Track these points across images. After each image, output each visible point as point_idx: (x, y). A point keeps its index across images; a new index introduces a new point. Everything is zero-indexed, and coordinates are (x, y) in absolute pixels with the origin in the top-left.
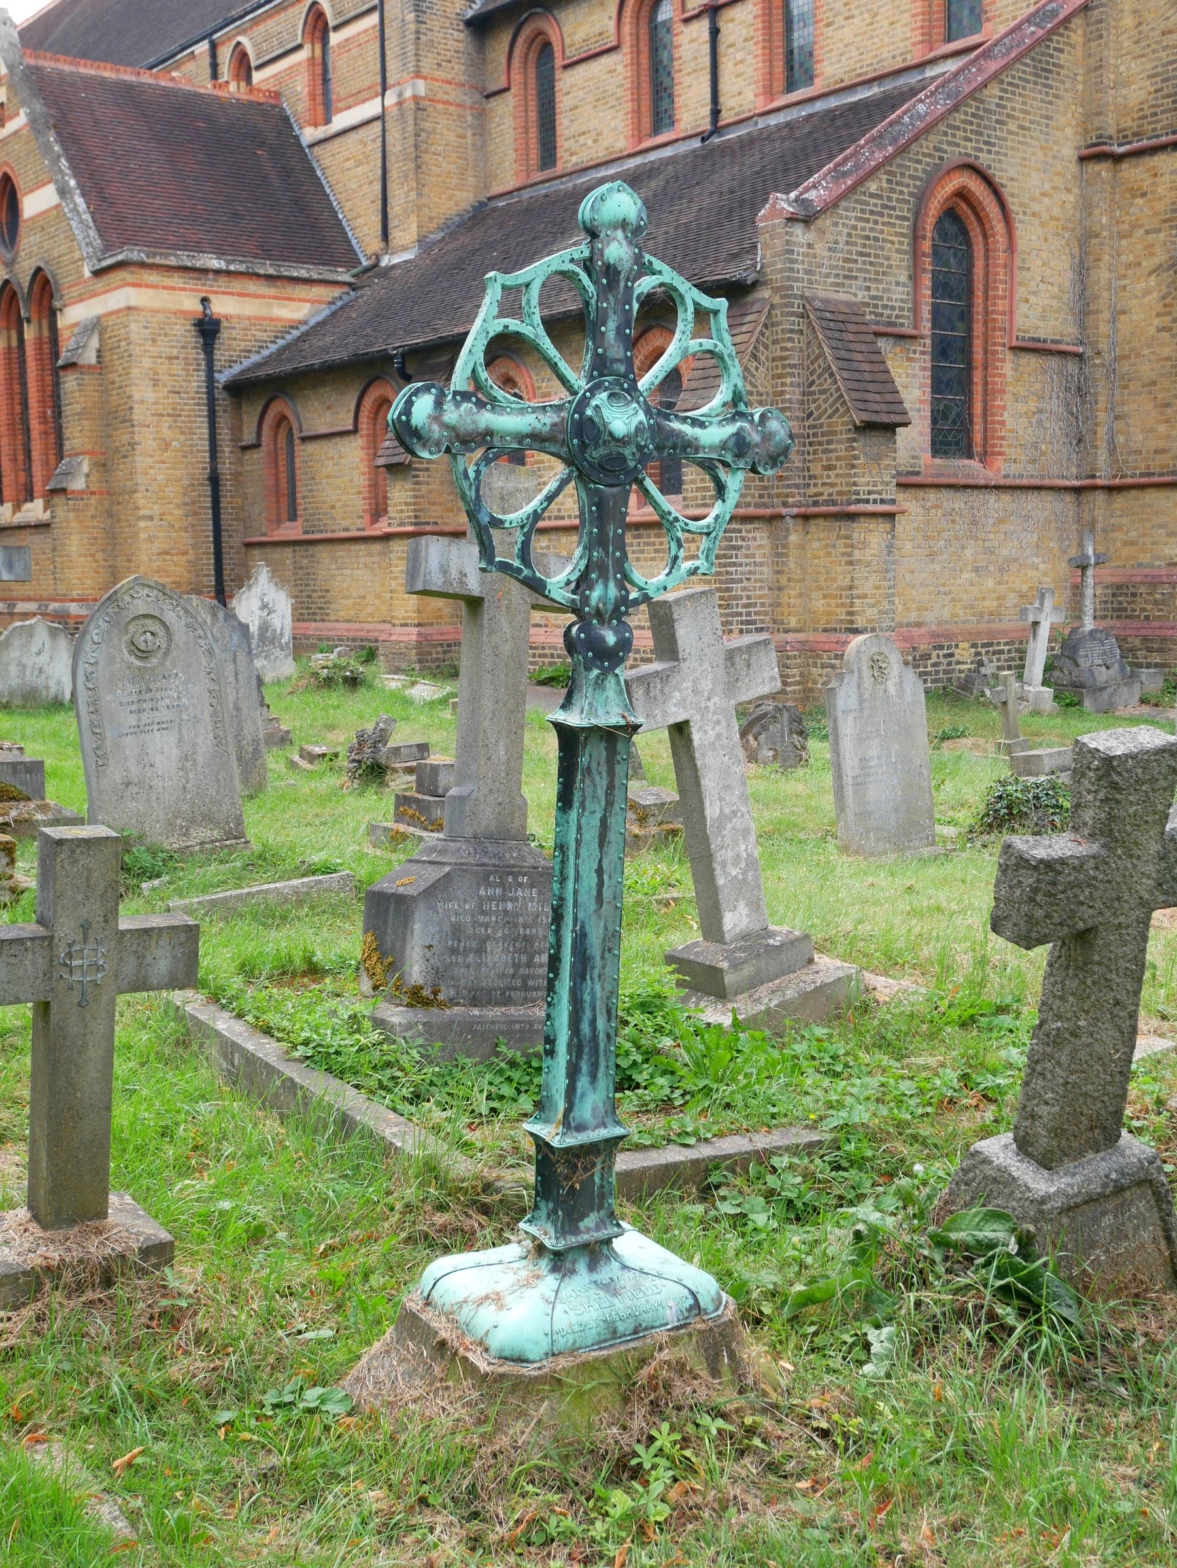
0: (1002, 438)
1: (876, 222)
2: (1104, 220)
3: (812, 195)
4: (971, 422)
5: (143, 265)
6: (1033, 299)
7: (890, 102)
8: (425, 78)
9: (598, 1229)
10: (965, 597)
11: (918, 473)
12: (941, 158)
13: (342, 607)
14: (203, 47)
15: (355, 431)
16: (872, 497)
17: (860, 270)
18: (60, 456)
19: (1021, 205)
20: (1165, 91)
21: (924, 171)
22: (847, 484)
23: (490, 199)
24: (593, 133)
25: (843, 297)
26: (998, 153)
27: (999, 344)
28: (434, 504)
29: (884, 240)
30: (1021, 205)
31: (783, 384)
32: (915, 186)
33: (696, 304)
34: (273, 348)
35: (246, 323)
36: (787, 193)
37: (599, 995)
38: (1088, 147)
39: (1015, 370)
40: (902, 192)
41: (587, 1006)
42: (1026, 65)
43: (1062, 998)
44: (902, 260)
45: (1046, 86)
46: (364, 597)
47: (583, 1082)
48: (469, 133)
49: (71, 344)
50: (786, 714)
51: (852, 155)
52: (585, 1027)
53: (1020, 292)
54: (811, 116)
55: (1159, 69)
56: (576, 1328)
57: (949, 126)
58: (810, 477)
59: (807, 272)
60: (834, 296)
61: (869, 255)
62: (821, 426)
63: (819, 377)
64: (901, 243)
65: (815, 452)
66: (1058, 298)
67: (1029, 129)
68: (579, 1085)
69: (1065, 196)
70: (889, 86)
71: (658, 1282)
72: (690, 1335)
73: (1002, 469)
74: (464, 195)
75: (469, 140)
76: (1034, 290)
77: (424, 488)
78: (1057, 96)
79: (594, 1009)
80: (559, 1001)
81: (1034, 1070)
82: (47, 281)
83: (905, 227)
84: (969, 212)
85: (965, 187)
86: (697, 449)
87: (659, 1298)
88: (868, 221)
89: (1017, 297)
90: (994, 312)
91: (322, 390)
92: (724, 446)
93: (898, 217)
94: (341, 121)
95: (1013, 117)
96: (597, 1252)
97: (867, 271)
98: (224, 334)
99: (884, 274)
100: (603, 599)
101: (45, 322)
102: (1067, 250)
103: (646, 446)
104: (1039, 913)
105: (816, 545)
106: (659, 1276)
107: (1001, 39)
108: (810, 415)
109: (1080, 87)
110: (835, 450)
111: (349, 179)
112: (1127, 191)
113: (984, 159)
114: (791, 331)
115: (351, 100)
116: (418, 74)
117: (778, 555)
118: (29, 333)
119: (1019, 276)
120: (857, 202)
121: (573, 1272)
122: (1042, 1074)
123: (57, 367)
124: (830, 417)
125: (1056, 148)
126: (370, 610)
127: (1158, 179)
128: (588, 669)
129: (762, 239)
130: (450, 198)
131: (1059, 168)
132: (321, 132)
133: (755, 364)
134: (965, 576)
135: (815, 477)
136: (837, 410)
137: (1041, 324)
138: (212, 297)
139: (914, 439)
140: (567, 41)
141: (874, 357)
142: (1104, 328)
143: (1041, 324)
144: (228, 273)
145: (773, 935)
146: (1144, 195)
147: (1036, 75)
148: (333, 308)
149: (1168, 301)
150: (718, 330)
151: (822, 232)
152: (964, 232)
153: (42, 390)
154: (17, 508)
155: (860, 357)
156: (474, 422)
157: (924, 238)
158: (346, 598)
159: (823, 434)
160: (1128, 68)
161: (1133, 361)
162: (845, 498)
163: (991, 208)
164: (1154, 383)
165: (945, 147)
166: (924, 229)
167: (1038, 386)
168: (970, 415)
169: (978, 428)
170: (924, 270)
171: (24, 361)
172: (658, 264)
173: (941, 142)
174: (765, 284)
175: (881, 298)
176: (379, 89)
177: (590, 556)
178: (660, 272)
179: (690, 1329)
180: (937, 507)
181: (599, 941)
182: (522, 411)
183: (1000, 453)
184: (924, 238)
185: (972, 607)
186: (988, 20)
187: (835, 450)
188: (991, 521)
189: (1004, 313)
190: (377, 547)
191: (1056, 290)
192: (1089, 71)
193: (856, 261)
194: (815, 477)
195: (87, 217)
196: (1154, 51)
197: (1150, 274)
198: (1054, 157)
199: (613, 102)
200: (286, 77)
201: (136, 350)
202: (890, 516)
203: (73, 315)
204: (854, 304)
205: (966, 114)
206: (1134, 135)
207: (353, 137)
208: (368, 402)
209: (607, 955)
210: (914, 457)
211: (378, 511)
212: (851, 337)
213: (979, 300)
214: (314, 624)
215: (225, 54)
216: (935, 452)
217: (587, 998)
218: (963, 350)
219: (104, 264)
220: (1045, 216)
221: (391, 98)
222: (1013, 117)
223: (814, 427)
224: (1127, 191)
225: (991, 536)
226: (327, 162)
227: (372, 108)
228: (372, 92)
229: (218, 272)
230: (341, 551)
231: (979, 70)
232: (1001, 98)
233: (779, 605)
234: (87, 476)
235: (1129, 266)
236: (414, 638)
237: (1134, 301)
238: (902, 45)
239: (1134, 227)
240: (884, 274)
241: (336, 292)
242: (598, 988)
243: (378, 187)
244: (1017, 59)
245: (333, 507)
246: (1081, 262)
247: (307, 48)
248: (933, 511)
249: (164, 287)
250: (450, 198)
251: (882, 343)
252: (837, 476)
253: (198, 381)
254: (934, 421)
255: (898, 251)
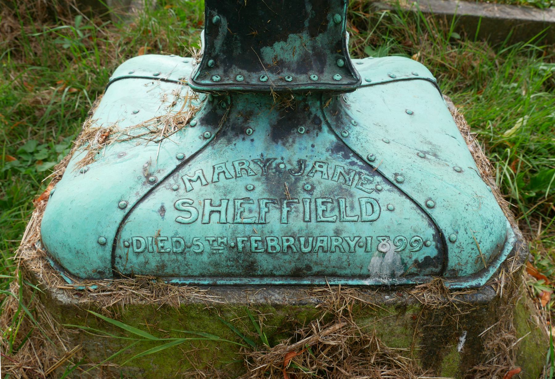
9: (303, 66)
56: (168, 246)
71: (388, 196)
72: (402, 308)
87: (366, 230)
96: (311, 109)
106: (395, 185)
121: (241, 131)
179: (407, 297)
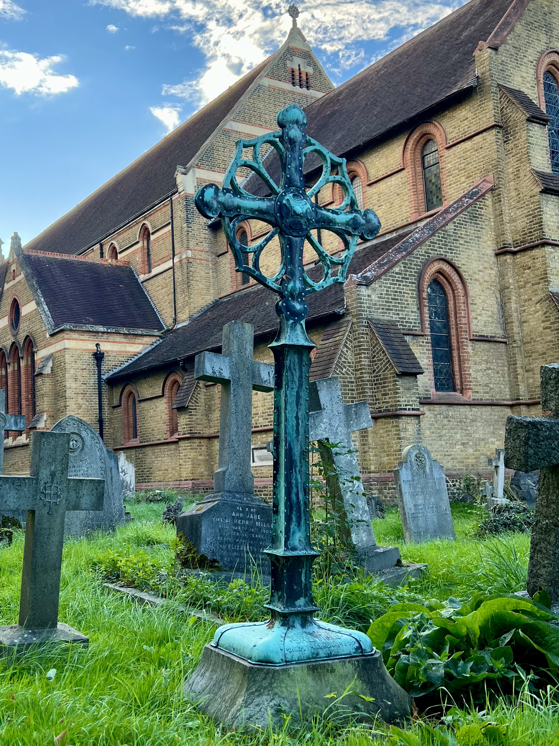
0: (470, 382)
1: (400, 285)
2: (511, 281)
3: (368, 274)
4: (454, 375)
5: (71, 330)
6: (479, 318)
7: (401, 237)
8: (191, 250)
10: (458, 457)
11: (430, 398)
12: (428, 256)
13: (158, 475)
14: (98, 246)
15: (162, 396)
16: (407, 407)
17: (394, 306)
18: (34, 413)
19: (469, 275)
20: (535, 222)
21: (421, 262)
22: (395, 401)
23: (220, 298)
24: (265, 267)
25: (386, 318)
26: (455, 253)
27: (464, 338)
28: (199, 424)
29: (404, 293)
30: (469, 275)
31: (360, 358)
32: (417, 269)
33: (331, 160)
34: (127, 364)
35: (115, 354)
36: (357, 274)
37: (299, 481)
38: (499, 249)
39: (473, 350)
40: (411, 272)
41: (294, 486)
42: (466, 215)
43: (547, 506)
44: (414, 301)
45: (476, 224)
46: (167, 470)
47: (293, 526)
48: (211, 271)
49: (41, 366)
50: (373, 501)
51: (386, 257)
52: (294, 497)
53: (472, 315)
54: (365, 248)
55: (531, 212)
57: (431, 242)
58: (376, 400)
59: (368, 307)
60: (382, 318)
61: (397, 299)
62: (380, 376)
63: (377, 353)
64: (412, 294)
65: (378, 388)
66: (492, 317)
67: (470, 242)
68: (292, 527)
69: (490, 272)
70: (401, 232)
73: (470, 396)
74: (209, 297)
75: (211, 274)
76: (480, 312)
77: (194, 417)
78: (482, 228)
79: (297, 487)
80: (280, 485)
81: (535, 549)
82: (31, 341)
83: (414, 287)
84: (444, 280)
85: (441, 269)
86: (335, 223)
88: (396, 284)
89: (471, 317)
90: (460, 324)
91: (148, 379)
92: (347, 224)
93: (410, 283)
94: (155, 271)
95: (462, 238)
97: (397, 307)
98: (106, 359)
99: (405, 307)
100: (294, 289)
101: (29, 358)
102: (494, 295)
103: (311, 220)
104: (531, 451)
105: (381, 431)
107: (453, 204)
108: (374, 371)
109: (493, 224)
110: (388, 386)
111: (159, 294)
112: (520, 267)
113: (449, 256)
114: (363, 334)
115: (160, 262)
116: (188, 248)
117: (363, 436)
118: (23, 363)
119: (471, 307)
120: (390, 276)
122: (540, 551)
123: (35, 375)
124: (384, 371)
125: (483, 250)
126: (170, 475)
127: (536, 261)
128: (288, 320)
129: (346, 294)
130: (203, 299)
131: (486, 259)
132: (147, 276)
133: (345, 349)
134: (457, 447)
135: (378, 399)
136: (387, 368)
137: (484, 329)
138: (100, 343)
139: (426, 381)
140: (253, 229)
141: (403, 344)
142: (516, 330)
143: (484, 329)
144: (108, 333)
145: (379, 548)
146: (529, 268)
147: (471, 219)
148: (153, 347)
149: (547, 315)
150: (343, 172)
151: (374, 290)
152: (442, 288)
153: (27, 387)
154: (14, 439)
155: (397, 344)
156: (232, 202)
157: (424, 291)
158: (160, 471)
159: (381, 379)
160: (515, 214)
161: (533, 344)
162: (394, 408)
163: (455, 278)
164: (545, 353)
165: (430, 251)
166: (423, 287)
167: (486, 357)
168: (453, 371)
169: (457, 377)
170: (425, 306)
171: (20, 376)
172: (313, 141)
173: (428, 249)
174: (348, 314)
175: (405, 318)
176: (172, 256)
177: (287, 268)
178: (314, 145)
180: (440, 414)
181: (298, 453)
182: (254, 199)
183: (470, 389)
184: (424, 291)
185: (462, 462)
186: (445, 200)
187: (388, 386)
188: (468, 421)
189: (466, 324)
190: (173, 447)
191: (490, 313)
192: (496, 216)
193: (391, 302)
194: (378, 399)
195: (48, 313)
196: (527, 205)
197: (537, 303)
198: (483, 254)
199: (274, 252)
200: (133, 256)
201: (68, 366)
202: (418, 416)
203: (40, 355)
204: (393, 321)
205: (439, 237)
206: (521, 242)
207: (161, 277)
208: (168, 383)
209: (302, 461)
210: (427, 391)
211: (173, 430)
212: (392, 335)
213: (452, 319)
214: (145, 484)
215: (106, 248)
216: (437, 389)
217: (294, 481)
218: (447, 342)
219: (55, 331)
220: (481, 280)
221: (176, 260)
222: (462, 238)
223: (377, 376)
224: (520, 267)
225: (469, 428)
226: (148, 289)
227: (169, 264)
228: (168, 258)
229: (103, 333)
230: (157, 449)
231: (444, 218)
232: (455, 230)
233: (365, 460)
234: (46, 421)
235: (525, 301)
236: (191, 485)
237: (530, 316)
238: (406, 215)
239: (526, 283)
240: (405, 307)
241: (154, 339)
242: (299, 477)
243: (172, 296)
244: (460, 213)
245: (153, 430)
246: (502, 300)
247: (141, 242)
248: (438, 416)
249: (80, 340)
250: (203, 299)
251: (407, 338)
252: (390, 398)
253: (93, 380)
254: (435, 374)
255: (411, 297)
